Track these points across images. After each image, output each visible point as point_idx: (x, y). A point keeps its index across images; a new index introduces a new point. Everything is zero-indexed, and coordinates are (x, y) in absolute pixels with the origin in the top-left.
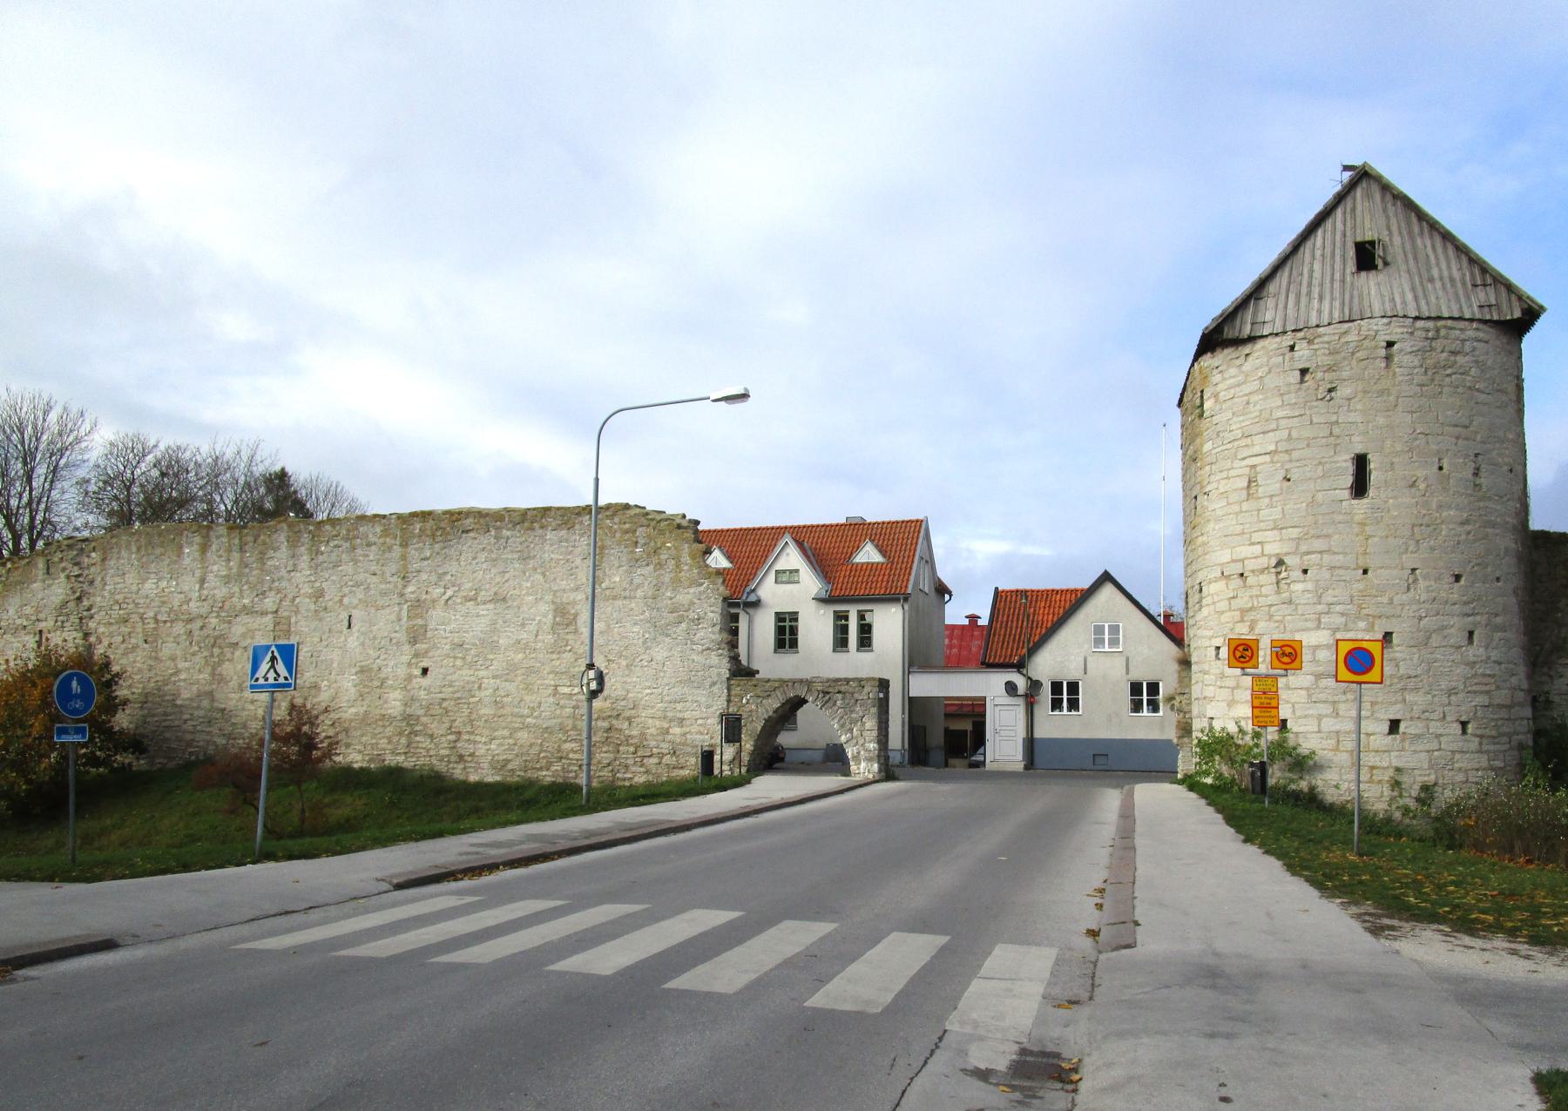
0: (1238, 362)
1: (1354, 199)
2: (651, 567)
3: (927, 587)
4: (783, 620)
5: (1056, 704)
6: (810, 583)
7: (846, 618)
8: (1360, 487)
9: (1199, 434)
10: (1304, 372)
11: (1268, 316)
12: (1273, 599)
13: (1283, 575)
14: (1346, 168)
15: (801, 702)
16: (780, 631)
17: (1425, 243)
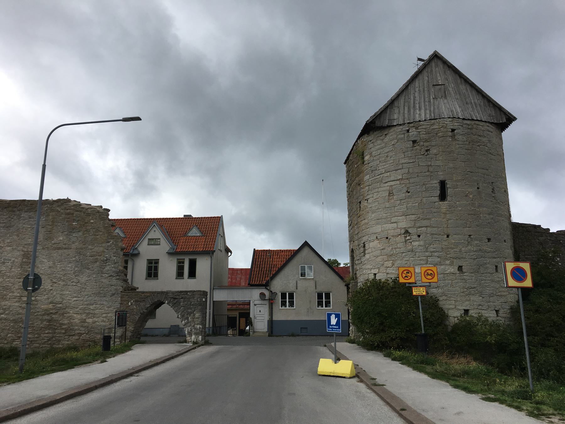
0: (381, 138)
1: (432, 67)
2: (80, 234)
3: (223, 249)
4: (152, 263)
5: (284, 304)
6: (165, 245)
7: (183, 263)
8: (443, 196)
9: (362, 172)
10: (414, 142)
11: (396, 116)
12: (403, 250)
13: (408, 238)
14: (419, 59)
15: (161, 303)
16: (149, 268)
17: (463, 87)
